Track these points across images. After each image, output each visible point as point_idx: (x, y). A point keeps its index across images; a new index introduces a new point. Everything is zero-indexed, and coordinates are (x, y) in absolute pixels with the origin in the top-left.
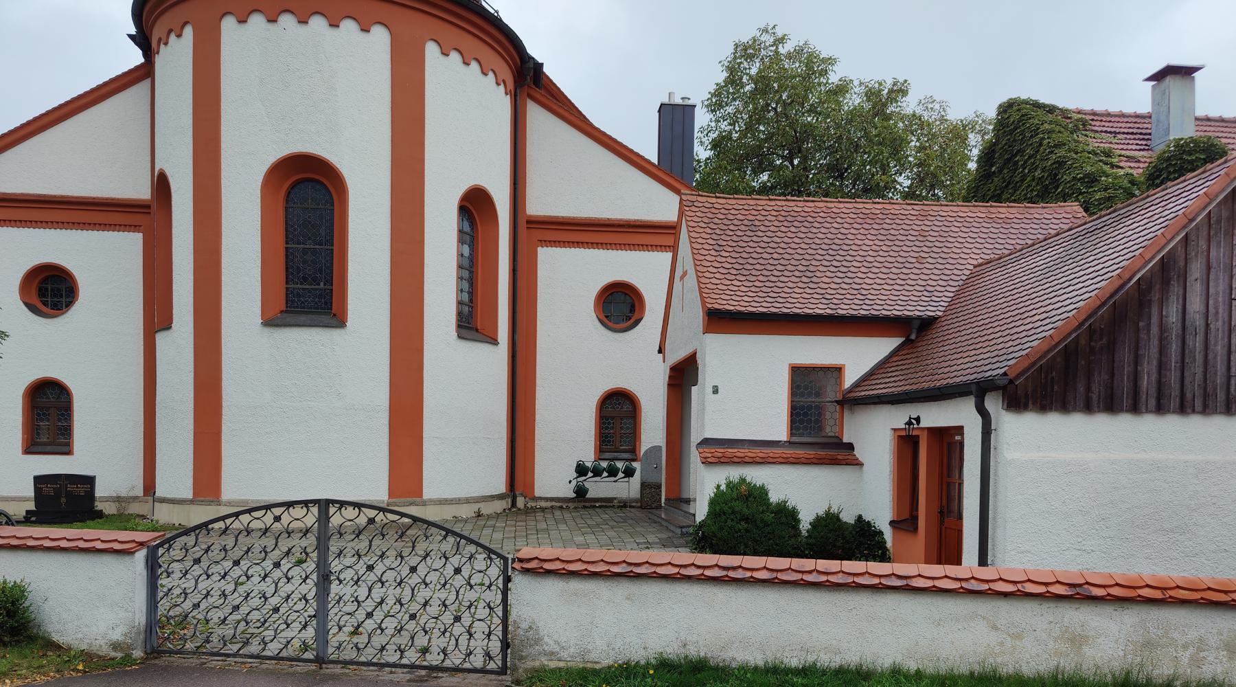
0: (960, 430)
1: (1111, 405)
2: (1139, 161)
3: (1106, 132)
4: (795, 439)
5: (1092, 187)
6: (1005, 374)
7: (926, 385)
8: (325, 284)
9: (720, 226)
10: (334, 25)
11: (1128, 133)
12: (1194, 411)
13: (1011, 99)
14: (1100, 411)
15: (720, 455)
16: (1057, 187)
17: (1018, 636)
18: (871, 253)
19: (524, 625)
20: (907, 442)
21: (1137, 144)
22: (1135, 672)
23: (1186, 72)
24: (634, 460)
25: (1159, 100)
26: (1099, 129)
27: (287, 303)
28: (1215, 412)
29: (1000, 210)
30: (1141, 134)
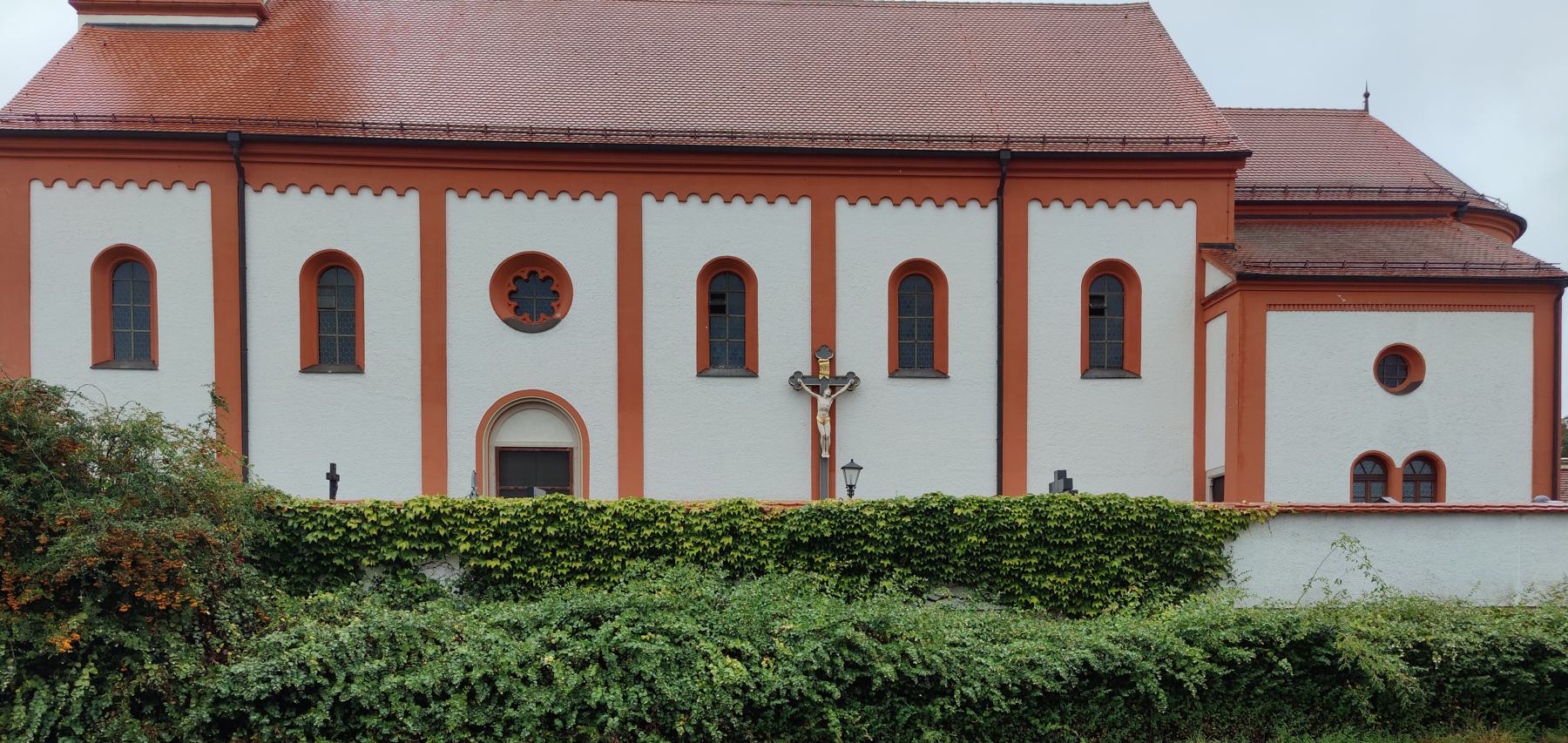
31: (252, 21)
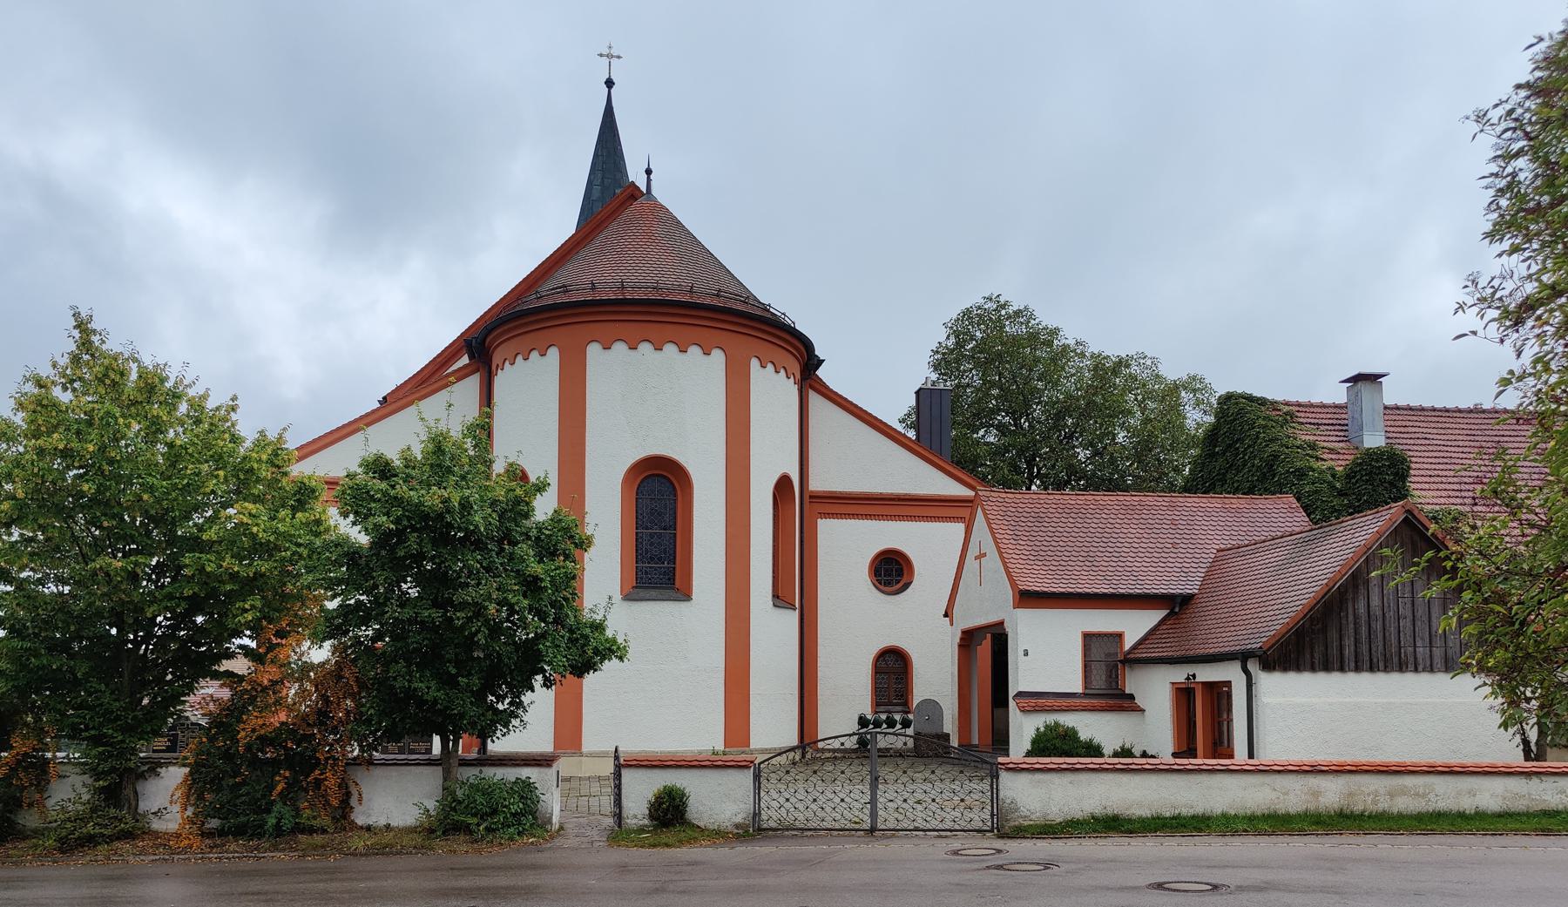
0: (1228, 684)
1: (1327, 667)
2: (1339, 453)
3: (1310, 423)
4: (1087, 691)
5: (1302, 480)
6: (1261, 648)
7: (1202, 652)
8: (668, 564)
9: (1013, 518)
10: (683, 351)
11: (1328, 425)
12: (1379, 670)
13: (1228, 393)
14: (1320, 670)
15: (1034, 705)
16: (1274, 476)
17: (1286, 794)
18: (1135, 540)
19: (1008, 801)
20: (1184, 695)
21: (1337, 436)
22: (1345, 808)
23: (1373, 379)
24: (909, 712)
25: (1354, 396)
26: (1304, 421)
27: (637, 580)
28: (1392, 670)
29: (1232, 501)
30: (1340, 425)
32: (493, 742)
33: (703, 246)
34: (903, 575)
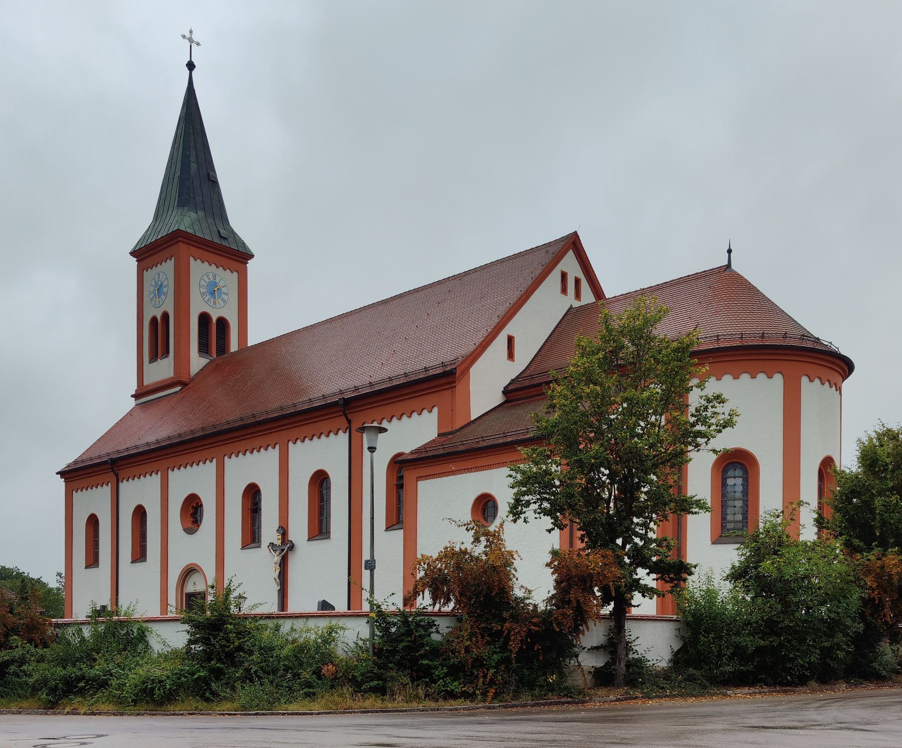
31: (178, 388)
32: (630, 635)
33: (782, 310)
34: (403, 488)
